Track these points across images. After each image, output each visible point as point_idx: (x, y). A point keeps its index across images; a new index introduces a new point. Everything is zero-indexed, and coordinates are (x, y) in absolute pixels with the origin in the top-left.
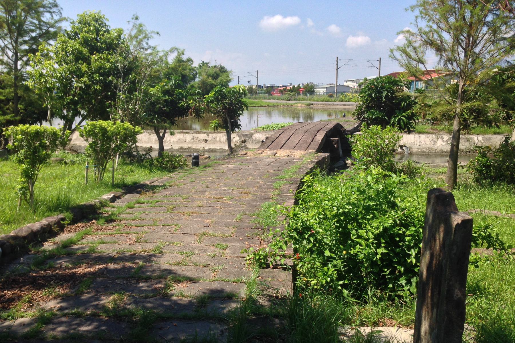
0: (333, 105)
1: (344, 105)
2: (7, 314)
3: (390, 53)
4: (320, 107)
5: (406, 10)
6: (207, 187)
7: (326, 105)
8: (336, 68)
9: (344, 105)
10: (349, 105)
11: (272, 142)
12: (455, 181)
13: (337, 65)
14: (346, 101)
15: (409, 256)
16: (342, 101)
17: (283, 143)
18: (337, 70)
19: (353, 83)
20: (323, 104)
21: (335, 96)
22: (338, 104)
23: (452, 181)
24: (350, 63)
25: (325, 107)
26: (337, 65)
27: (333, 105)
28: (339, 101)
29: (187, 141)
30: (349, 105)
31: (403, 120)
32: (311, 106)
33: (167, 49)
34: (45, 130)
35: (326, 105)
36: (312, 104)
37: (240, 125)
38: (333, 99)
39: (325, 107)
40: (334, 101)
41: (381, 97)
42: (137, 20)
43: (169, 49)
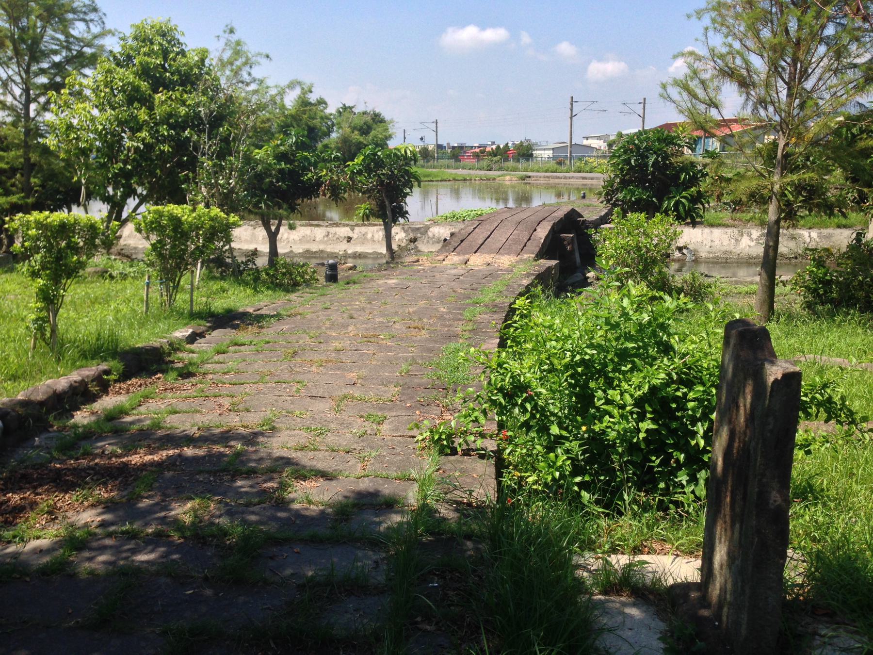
0: (565, 178)
1: (584, 178)
3: (661, 91)
4: (542, 181)
6: (352, 318)
7: (553, 178)
8: (569, 115)
9: (584, 178)
10: (592, 179)
12: (771, 307)
13: (572, 110)
14: (587, 172)
16: (580, 172)
17: (480, 242)
18: (571, 118)
19: (598, 141)
20: (548, 177)
21: (568, 162)
22: (573, 177)
23: (766, 308)
25: (552, 181)
26: (572, 110)
27: (565, 178)
28: (574, 172)
29: (317, 239)
32: (528, 181)
33: (284, 83)
34: (76, 220)
35: (553, 178)
36: (530, 177)
37: (407, 212)
39: (552, 181)
40: (567, 172)
41: (647, 165)
42: (232, 35)
43: (287, 83)
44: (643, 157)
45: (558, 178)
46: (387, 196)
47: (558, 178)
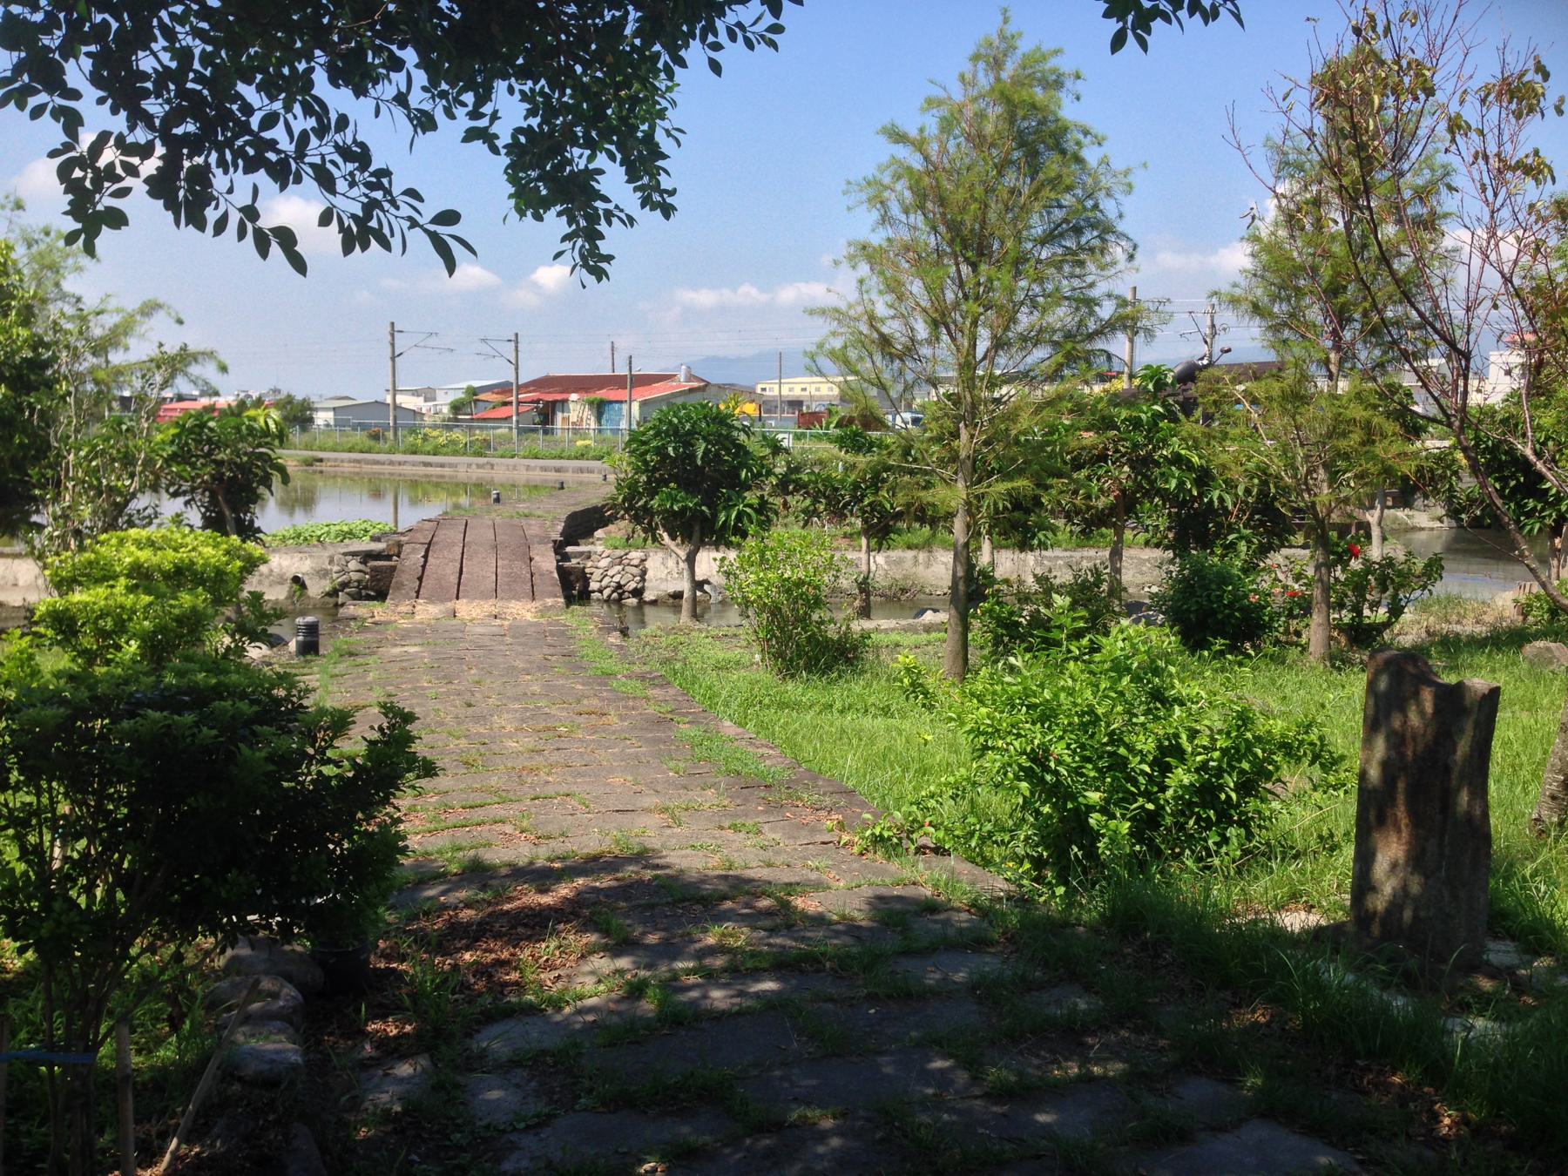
0: (391, 463)
1: (426, 464)
2: (779, 941)
3: (808, 360)
4: (347, 468)
5: (836, 263)
6: (470, 705)
7: (368, 462)
8: (389, 354)
9: (426, 464)
10: (442, 466)
11: (420, 579)
12: (966, 660)
13: (393, 345)
14: (428, 453)
15: (1221, 788)
16: (414, 453)
17: (454, 579)
18: (393, 359)
19: (415, 399)
20: (358, 461)
21: (390, 435)
22: (405, 463)
23: (960, 662)
24: (432, 341)
25: (367, 468)
26: (393, 345)
27: (391, 463)
28: (404, 453)
29: (21, 583)
30: (442, 466)
31: (749, 515)
32: (318, 467)
33: (133, 304)
34: (175, 565)
35: (368, 462)
36: (321, 460)
37: (259, 530)
38: (381, 444)
39: (367, 468)
40: (390, 452)
41: (693, 456)
42: (20, 212)
43: (137, 305)
44: (686, 440)
45: (377, 463)
46: (228, 502)
47: (377, 463)
